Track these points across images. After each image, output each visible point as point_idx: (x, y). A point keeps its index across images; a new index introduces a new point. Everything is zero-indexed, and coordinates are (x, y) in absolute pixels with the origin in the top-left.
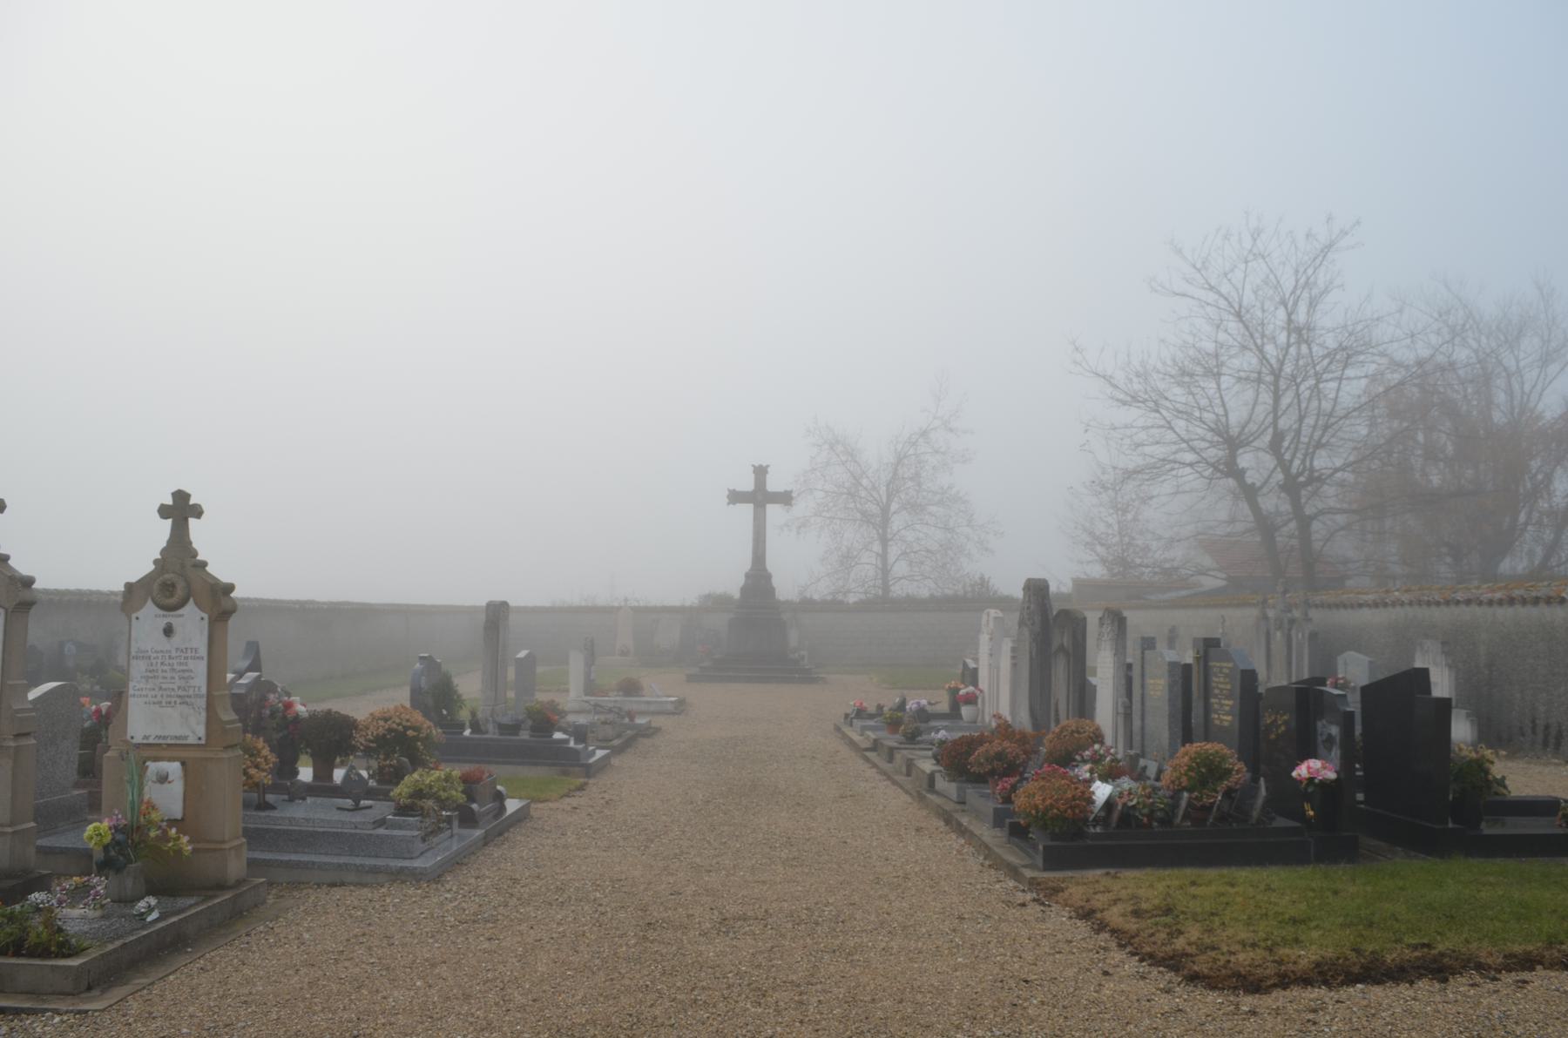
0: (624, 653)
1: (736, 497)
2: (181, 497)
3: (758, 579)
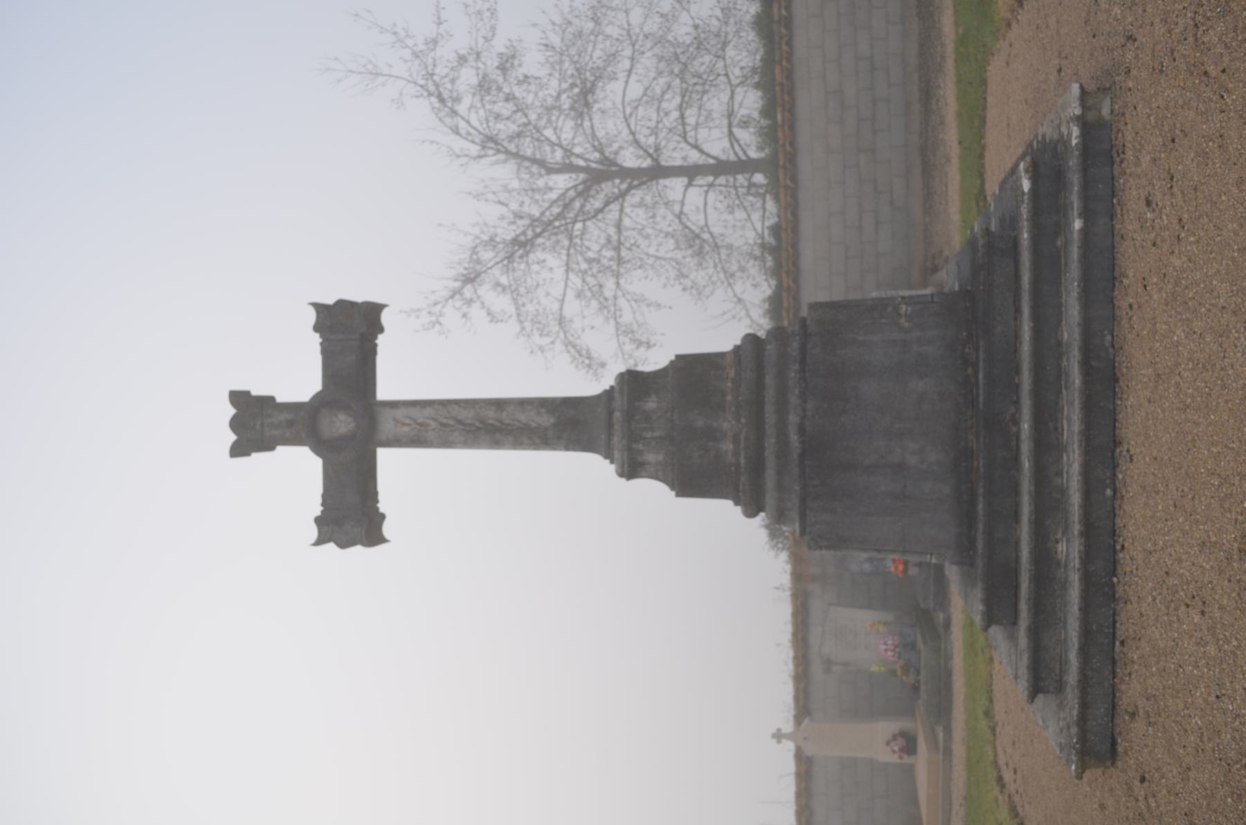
0: (909, 744)
1: (351, 515)
2: (774, 736)
3: (664, 425)
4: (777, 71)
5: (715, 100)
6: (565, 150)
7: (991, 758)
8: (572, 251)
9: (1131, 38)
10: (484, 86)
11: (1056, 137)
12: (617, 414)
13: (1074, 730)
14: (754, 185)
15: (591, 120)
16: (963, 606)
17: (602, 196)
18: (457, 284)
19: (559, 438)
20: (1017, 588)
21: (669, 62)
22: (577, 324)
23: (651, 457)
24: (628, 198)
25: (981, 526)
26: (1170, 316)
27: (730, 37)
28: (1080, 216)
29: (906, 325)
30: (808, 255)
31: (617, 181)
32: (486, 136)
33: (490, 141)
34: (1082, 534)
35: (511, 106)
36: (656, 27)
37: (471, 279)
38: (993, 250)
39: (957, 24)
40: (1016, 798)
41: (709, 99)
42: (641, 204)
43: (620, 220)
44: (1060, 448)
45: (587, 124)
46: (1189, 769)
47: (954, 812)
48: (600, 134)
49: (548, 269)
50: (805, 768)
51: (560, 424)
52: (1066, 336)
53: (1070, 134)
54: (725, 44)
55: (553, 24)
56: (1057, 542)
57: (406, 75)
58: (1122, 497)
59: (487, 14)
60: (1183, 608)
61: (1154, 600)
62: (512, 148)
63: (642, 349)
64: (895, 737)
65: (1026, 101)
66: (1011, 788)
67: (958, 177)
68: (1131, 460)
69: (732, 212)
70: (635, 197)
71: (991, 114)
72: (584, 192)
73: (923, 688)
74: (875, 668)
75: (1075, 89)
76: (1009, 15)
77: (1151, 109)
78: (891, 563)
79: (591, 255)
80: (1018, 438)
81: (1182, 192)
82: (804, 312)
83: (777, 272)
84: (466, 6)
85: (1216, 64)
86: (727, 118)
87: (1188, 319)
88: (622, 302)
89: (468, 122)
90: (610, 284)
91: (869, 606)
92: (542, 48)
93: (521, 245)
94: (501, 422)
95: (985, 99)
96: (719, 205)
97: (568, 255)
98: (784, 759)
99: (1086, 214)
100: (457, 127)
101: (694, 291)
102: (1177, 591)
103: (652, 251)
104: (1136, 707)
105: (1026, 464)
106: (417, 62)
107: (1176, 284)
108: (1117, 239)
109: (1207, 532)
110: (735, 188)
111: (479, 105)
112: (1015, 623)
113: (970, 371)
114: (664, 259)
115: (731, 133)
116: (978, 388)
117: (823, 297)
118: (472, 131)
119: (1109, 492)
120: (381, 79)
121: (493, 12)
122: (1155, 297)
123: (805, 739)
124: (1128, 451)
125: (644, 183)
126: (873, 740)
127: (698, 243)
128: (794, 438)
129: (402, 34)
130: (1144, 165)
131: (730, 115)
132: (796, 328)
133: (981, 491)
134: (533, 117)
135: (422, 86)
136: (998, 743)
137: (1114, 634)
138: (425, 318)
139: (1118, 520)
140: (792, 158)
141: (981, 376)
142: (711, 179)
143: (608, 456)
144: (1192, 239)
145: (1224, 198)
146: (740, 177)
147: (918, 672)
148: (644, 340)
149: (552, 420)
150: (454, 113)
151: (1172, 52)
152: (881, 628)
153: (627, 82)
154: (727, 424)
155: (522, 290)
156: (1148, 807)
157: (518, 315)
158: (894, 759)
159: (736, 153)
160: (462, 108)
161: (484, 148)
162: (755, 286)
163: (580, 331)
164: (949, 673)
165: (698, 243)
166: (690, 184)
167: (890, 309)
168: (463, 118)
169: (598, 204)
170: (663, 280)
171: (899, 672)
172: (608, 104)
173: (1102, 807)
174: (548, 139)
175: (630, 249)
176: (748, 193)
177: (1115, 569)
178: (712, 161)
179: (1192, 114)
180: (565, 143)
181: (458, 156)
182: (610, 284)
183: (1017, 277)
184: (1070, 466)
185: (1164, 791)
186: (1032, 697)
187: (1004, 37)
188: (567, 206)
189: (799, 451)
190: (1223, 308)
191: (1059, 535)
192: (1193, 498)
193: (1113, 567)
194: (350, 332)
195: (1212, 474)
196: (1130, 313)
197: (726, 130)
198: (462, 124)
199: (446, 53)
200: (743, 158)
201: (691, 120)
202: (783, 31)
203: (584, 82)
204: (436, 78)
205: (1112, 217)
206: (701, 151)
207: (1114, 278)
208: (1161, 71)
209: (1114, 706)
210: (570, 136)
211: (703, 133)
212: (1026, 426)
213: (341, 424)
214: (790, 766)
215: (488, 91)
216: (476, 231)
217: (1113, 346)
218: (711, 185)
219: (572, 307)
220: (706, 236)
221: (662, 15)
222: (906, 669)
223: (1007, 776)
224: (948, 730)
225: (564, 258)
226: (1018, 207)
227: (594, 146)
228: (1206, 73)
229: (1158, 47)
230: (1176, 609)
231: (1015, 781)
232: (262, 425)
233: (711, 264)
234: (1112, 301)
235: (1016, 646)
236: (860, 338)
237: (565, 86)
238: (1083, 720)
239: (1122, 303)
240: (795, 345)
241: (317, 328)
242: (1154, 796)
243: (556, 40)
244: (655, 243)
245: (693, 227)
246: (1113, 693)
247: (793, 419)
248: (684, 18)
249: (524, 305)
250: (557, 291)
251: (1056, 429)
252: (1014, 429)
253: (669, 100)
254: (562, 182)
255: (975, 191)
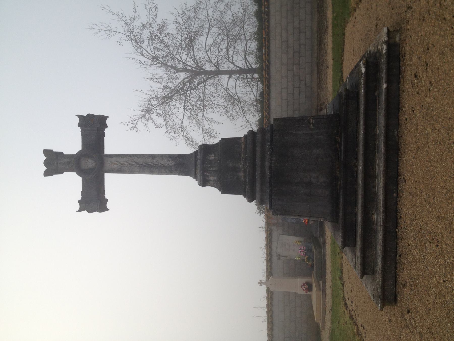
0: (310, 288)
2: (259, 283)
3: (216, 166)
4: (264, 33)
5: (240, 46)
6: (184, 63)
7: (342, 296)
8: (186, 102)
9: (410, 8)
10: (153, 37)
11: (375, 51)
12: (199, 161)
13: (380, 290)
14: (254, 78)
15: (193, 52)
16: (330, 236)
17: (197, 81)
18: (143, 113)
19: (176, 170)
20: (356, 232)
21: (223, 30)
22: (188, 129)
23: (212, 178)
24: (207, 83)
25: (341, 207)
26: (425, 123)
27: (246, 21)
28: (386, 82)
29: (313, 127)
30: (274, 103)
31: (203, 76)
32: (154, 57)
33: (155, 58)
34: (383, 211)
35: (163, 45)
36: (218, 16)
37: (148, 111)
38: (348, 97)
39: (333, 12)
40: (353, 312)
41: (238, 45)
42: (212, 85)
43: (204, 91)
44: (374, 177)
45: (192, 53)
46: (430, 310)
47: (327, 314)
48: (197, 58)
49: (177, 108)
50: (270, 295)
51: (176, 165)
52: (378, 132)
53: (382, 49)
54: (244, 23)
55: (179, 13)
56: (373, 214)
57: (122, 32)
58: (401, 197)
59: (154, 9)
60: (428, 243)
61: (415, 239)
62: (164, 62)
63: (212, 139)
64: (304, 285)
65: (361, 40)
66: (351, 308)
67: (332, 73)
68: (405, 182)
69: (245, 88)
70: (210, 82)
71: (347, 47)
72: (191, 79)
73: (315, 266)
74: (297, 258)
75: (385, 30)
76: (355, 6)
77: (418, 36)
78: (304, 220)
79: (193, 103)
80: (357, 172)
81: (432, 70)
82: (272, 122)
83: (262, 110)
84: (146, 5)
85: (450, 14)
86: (244, 54)
87: (433, 124)
88: (205, 121)
89: (147, 51)
90: (200, 115)
91: (295, 235)
92: (175, 23)
93: (167, 99)
94: (153, 163)
95: (344, 41)
96: (241, 85)
97: (185, 103)
98: (263, 290)
99: (388, 82)
100: (142, 53)
101: (231, 118)
102: (425, 236)
103: (216, 102)
104: (406, 282)
105: (360, 183)
106: (127, 27)
107: (428, 109)
108: (401, 92)
109: (440, 212)
110: (247, 79)
111: (151, 44)
112: (354, 245)
113: (337, 146)
114: (220, 105)
115: (245, 58)
116: (341, 153)
117: (279, 116)
118: (148, 54)
119: (395, 195)
120: (113, 33)
121: (156, 8)
122: (418, 115)
123: (270, 284)
124: (404, 178)
125: (213, 76)
126: (296, 285)
127: (233, 99)
128: (268, 171)
129: (121, 15)
130: (414, 61)
131: (246, 51)
132: (269, 128)
133: (341, 193)
134: (171, 49)
135: (128, 36)
136: (345, 289)
137: (396, 252)
138: (131, 126)
139: (399, 206)
140: (268, 67)
141: (342, 148)
142: (238, 75)
143: (195, 177)
144: (436, 90)
145: (452, 72)
146: (249, 75)
147: (313, 261)
148: (213, 135)
149: (173, 163)
150: (141, 47)
151: (429, 11)
152: (299, 244)
153: (207, 38)
154: (241, 166)
155: (168, 116)
156: (411, 323)
157: (166, 125)
158: (304, 293)
159: (248, 67)
160: (144, 45)
161: (153, 61)
162: (254, 116)
163: (189, 132)
164: (325, 261)
165: (233, 99)
166: (230, 77)
167: (306, 121)
168: (145, 49)
169: (195, 84)
170: (220, 113)
171: (306, 260)
172: (200, 46)
173: (390, 321)
174: (177, 59)
175: (207, 101)
176: (252, 81)
177: (397, 226)
178: (238, 69)
179: (437, 37)
180: (183, 60)
181: (143, 64)
182: (200, 115)
183: (358, 108)
184: (379, 184)
185: (418, 317)
186: (362, 277)
187: (353, 16)
188: (184, 85)
189: (269, 176)
190: (450, 118)
191: (374, 212)
192: (434, 198)
193: (396, 225)
194: (93, 127)
195: (443, 188)
196: (406, 122)
197: (244, 57)
198: (145, 52)
199: (138, 23)
200: (250, 68)
201: (231, 53)
202: (266, 17)
203: (191, 37)
204: (134, 33)
205: (399, 82)
206: (235, 65)
207: (399, 108)
208: (424, 20)
209: (396, 281)
210: (185, 58)
211: (235, 58)
212: (361, 168)
213: (89, 163)
214: (265, 294)
215: (154, 39)
216: (150, 93)
217: (398, 136)
218: (238, 78)
219: (186, 123)
220: (236, 97)
221: (220, 12)
222: (308, 259)
223: (349, 303)
224: (324, 283)
225: (183, 104)
226: (359, 79)
227: (194, 62)
228: (445, 19)
229: (423, 10)
230: (425, 243)
231: (352, 306)
232: (57, 163)
233: (238, 108)
234: (398, 118)
235: (355, 255)
236: (294, 132)
237: (183, 38)
238: (383, 287)
239: (403, 118)
240: (269, 135)
241: (79, 125)
242: (413, 319)
243: (180, 20)
244: (217, 99)
245: (231, 94)
246: (396, 275)
247: (267, 164)
248: (229, 12)
249: (168, 121)
250: (181, 117)
251: (373, 169)
252: (356, 169)
253: (223, 45)
254: (182, 75)
255: (339, 78)
